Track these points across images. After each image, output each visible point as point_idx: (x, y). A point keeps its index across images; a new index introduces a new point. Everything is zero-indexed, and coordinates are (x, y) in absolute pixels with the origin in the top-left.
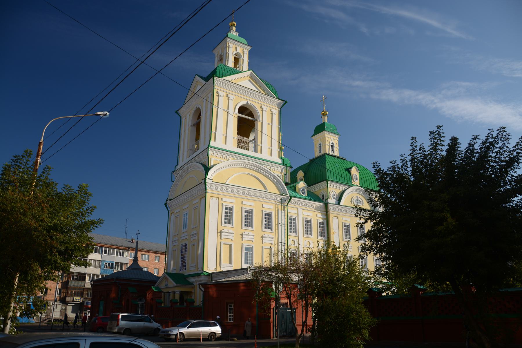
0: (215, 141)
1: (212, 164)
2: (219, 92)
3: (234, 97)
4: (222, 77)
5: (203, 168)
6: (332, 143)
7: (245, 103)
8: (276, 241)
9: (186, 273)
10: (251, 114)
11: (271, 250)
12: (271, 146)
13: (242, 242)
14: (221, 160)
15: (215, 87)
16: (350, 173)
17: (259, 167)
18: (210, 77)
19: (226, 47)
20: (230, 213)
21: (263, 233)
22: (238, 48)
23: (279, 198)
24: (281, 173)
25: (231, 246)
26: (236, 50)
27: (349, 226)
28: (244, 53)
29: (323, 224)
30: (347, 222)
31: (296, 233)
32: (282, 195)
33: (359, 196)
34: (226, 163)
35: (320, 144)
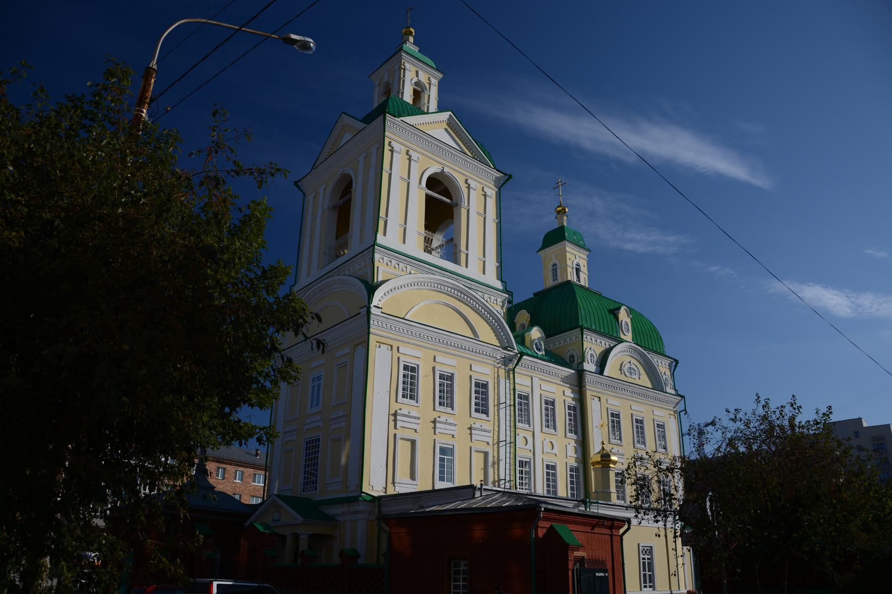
0: (385, 234)
1: (380, 279)
2: (394, 144)
3: (420, 156)
4: (400, 116)
5: (362, 287)
6: (578, 265)
7: (439, 171)
8: (496, 438)
9: (317, 496)
10: (446, 193)
11: (486, 454)
12: (484, 256)
13: (435, 437)
14: (394, 271)
15: (386, 133)
16: (617, 318)
17: (465, 294)
18: (381, 111)
19: (399, 69)
20: (412, 377)
21: (472, 421)
22: (420, 73)
23: (501, 354)
24: (502, 307)
25: (413, 443)
26: (417, 76)
27: (618, 416)
28: (430, 84)
29: (574, 409)
30: (616, 408)
31: (529, 424)
32: (505, 348)
33: (633, 361)
34: (406, 279)
35: (555, 265)
